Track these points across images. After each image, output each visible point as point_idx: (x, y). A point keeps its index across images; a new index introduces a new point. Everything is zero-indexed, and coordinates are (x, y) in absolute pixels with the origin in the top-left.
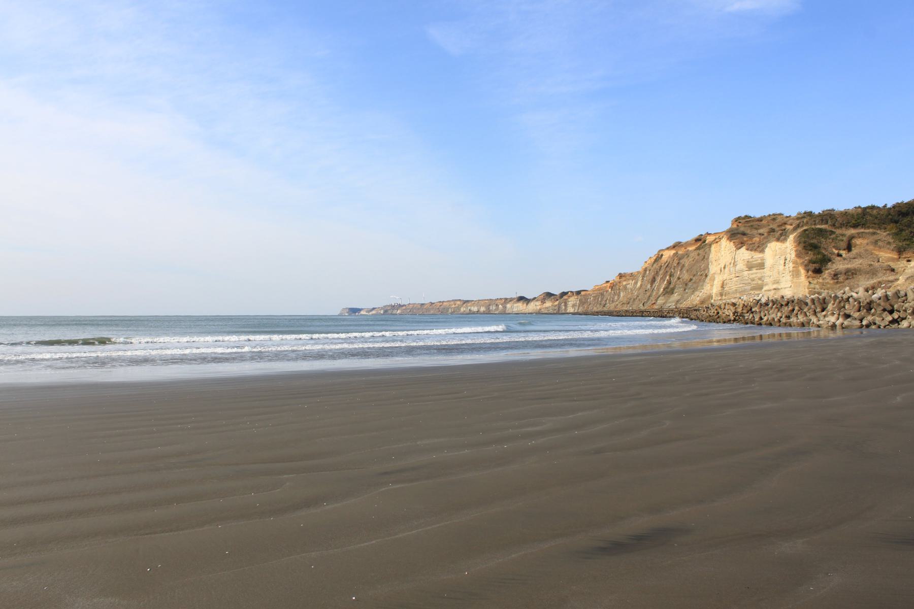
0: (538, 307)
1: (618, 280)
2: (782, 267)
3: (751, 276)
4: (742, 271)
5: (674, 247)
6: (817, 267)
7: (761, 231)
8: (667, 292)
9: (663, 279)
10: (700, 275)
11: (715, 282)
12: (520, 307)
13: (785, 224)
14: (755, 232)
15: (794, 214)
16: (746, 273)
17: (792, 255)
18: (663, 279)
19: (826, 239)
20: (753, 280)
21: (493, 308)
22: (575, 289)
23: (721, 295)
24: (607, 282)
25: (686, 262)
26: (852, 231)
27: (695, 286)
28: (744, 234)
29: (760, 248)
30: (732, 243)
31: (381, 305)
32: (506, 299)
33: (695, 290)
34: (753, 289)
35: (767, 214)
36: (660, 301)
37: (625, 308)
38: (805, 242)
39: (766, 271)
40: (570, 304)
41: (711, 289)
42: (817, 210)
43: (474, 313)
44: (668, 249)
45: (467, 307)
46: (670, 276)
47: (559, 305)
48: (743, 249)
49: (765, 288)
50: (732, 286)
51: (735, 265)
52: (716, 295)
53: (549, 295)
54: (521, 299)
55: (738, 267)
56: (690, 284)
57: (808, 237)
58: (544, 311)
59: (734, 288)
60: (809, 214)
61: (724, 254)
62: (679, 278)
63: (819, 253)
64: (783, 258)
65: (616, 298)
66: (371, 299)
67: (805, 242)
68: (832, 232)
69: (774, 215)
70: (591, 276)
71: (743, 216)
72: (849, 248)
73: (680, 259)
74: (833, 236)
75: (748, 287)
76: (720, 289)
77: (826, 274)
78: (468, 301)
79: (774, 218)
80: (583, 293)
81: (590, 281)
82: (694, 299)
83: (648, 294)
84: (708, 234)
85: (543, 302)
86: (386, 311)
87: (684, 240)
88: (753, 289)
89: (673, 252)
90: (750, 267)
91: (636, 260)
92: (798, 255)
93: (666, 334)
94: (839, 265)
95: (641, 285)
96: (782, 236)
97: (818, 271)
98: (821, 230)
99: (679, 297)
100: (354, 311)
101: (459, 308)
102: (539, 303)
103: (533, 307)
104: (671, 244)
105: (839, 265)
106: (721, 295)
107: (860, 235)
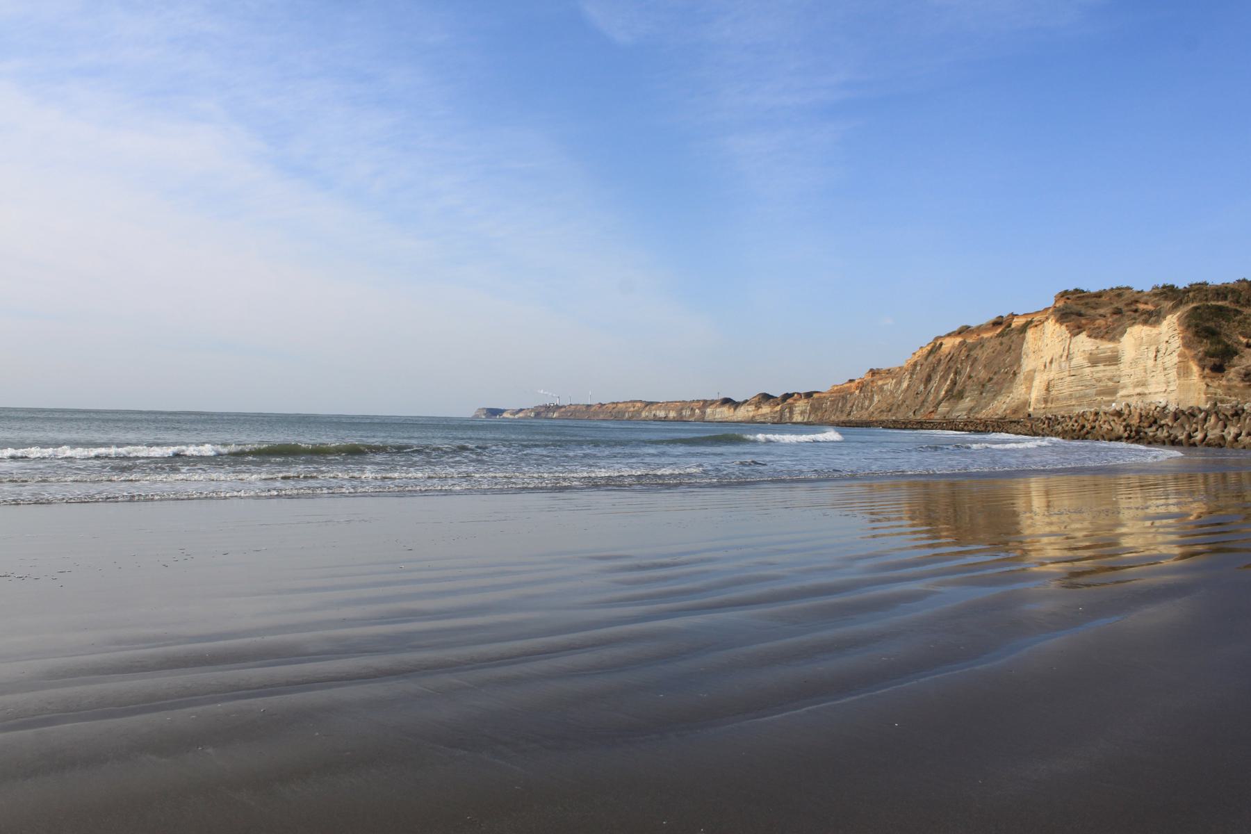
0: (751, 414)
1: (869, 378)
2: (1151, 363)
3: (1096, 376)
4: (1082, 367)
5: (959, 333)
6: (1217, 361)
7: (1102, 311)
8: (952, 396)
9: (944, 378)
11: (1036, 383)
12: (725, 413)
13: (1137, 302)
16: (1088, 370)
17: (1177, 343)
18: (944, 378)
19: (1228, 320)
20: (1099, 380)
22: (803, 390)
23: (1046, 401)
24: (851, 381)
25: (982, 355)
27: (996, 388)
28: (1080, 315)
29: (1111, 333)
30: (1063, 327)
31: (531, 406)
32: (705, 401)
34: (1099, 393)
35: (1108, 288)
36: (943, 409)
37: (884, 418)
38: (1197, 326)
39: (1124, 368)
40: (797, 410)
43: (660, 420)
44: (949, 335)
45: (650, 411)
46: (956, 373)
47: (782, 412)
48: (1083, 336)
49: (1121, 393)
51: (1069, 357)
52: (1038, 401)
53: (766, 398)
54: (726, 401)
55: (1074, 362)
56: (989, 385)
57: (1201, 319)
58: (759, 419)
59: (1066, 392)
62: (970, 377)
63: (1219, 342)
64: (1153, 348)
65: (867, 403)
67: (1197, 326)
68: (1238, 312)
69: (1118, 288)
70: (829, 371)
71: (1071, 289)
73: (970, 350)
74: (1238, 318)
75: (1093, 391)
76: (1044, 392)
77: (1232, 373)
78: (651, 403)
79: (1119, 292)
80: (815, 396)
81: (824, 384)
82: (1000, 406)
83: (921, 398)
84: (1014, 315)
85: (758, 407)
86: (538, 415)
88: (1099, 393)
89: (958, 340)
90: (1094, 361)
92: (1187, 344)
95: (909, 386)
96: (1151, 318)
97: (1218, 369)
98: (1220, 308)
99: (972, 404)
100: (494, 412)
102: (751, 408)
103: (743, 413)
104: (956, 328)
106: (1046, 401)
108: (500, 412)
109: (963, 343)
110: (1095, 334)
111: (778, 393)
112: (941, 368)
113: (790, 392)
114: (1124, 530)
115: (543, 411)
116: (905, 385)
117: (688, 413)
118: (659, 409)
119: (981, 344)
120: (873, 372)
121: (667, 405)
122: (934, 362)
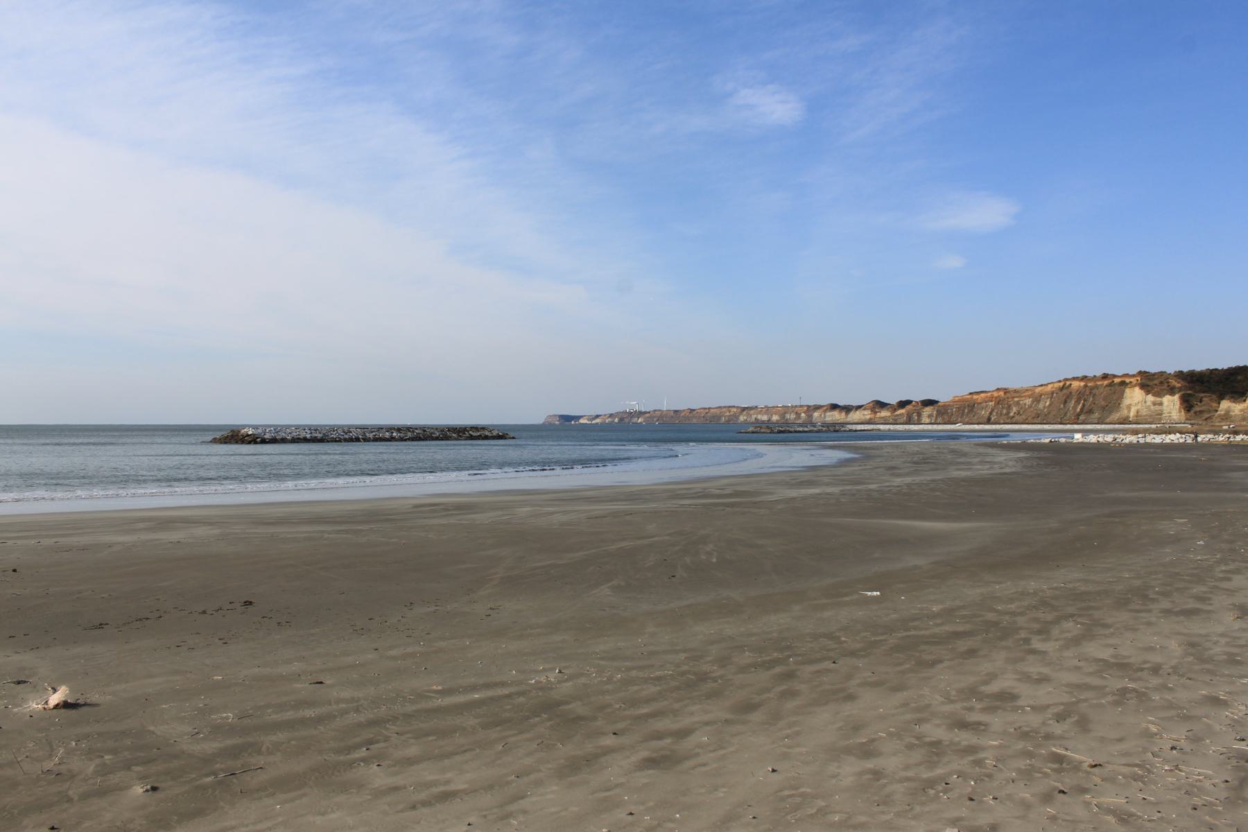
9: (1078, 402)
18: (1078, 402)
32: (809, 407)
33: (1111, 412)
42: (1185, 370)
53: (881, 405)
54: (834, 407)
60: (1181, 372)
66: (592, 404)
79: (1162, 373)
86: (621, 420)
89: (1082, 384)
90: (1154, 404)
93: (673, 492)
94: (1197, 409)
101: (736, 416)
104: (1080, 375)
105: (1197, 409)
108: (579, 417)
109: (1086, 386)
110: (1154, 395)
111: (893, 401)
114: (549, 724)
115: (1230, 369)
117: (793, 416)
119: (1097, 387)
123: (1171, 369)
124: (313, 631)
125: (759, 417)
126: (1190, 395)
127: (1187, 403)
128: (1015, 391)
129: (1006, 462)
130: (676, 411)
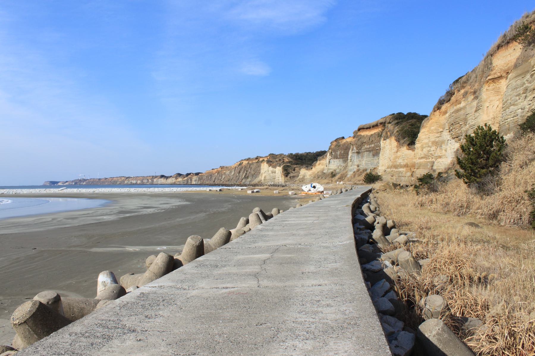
0: (174, 181)
9: (244, 172)
10: (257, 173)
12: (163, 181)
14: (275, 160)
15: (287, 154)
18: (244, 172)
21: (145, 181)
22: (194, 172)
26: (295, 166)
32: (153, 176)
33: (256, 178)
36: (243, 181)
39: (276, 174)
40: (193, 180)
41: (261, 178)
42: (294, 153)
44: (245, 160)
45: (129, 181)
47: (187, 180)
50: (268, 178)
53: (179, 175)
54: (162, 176)
60: (291, 154)
61: (265, 167)
72: (294, 170)
77: (289, 177)
81: (204, 170)
82: (256, 181)
85: (176, 178)
87: (252, 157)
89: (247, 162)
90: (272, 172)
91: (232, 162)
97: (287, 176)
102: (174, 179)
104: (247, 158)
105: (291, 175)
107: (297, 167)
108: (58, 182)
109: (248, 163)
112: (243, 169)
113: (189, 173)
116: (233, 173)
117: (146, 181)
118: (133, 180)
119: (253, 164)
120: (222, 168)
121: (136, 178)
122: (240, 167)
123: (286, 153)
124: (252, 283)
125: (132, 181)
126: (288, 166)
127: (286, 172)
128: (227, 167)
129: (176, 203)
130: (100, 179)
